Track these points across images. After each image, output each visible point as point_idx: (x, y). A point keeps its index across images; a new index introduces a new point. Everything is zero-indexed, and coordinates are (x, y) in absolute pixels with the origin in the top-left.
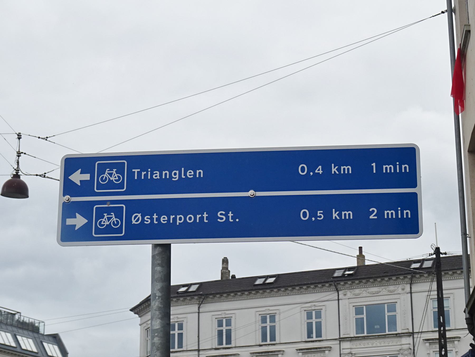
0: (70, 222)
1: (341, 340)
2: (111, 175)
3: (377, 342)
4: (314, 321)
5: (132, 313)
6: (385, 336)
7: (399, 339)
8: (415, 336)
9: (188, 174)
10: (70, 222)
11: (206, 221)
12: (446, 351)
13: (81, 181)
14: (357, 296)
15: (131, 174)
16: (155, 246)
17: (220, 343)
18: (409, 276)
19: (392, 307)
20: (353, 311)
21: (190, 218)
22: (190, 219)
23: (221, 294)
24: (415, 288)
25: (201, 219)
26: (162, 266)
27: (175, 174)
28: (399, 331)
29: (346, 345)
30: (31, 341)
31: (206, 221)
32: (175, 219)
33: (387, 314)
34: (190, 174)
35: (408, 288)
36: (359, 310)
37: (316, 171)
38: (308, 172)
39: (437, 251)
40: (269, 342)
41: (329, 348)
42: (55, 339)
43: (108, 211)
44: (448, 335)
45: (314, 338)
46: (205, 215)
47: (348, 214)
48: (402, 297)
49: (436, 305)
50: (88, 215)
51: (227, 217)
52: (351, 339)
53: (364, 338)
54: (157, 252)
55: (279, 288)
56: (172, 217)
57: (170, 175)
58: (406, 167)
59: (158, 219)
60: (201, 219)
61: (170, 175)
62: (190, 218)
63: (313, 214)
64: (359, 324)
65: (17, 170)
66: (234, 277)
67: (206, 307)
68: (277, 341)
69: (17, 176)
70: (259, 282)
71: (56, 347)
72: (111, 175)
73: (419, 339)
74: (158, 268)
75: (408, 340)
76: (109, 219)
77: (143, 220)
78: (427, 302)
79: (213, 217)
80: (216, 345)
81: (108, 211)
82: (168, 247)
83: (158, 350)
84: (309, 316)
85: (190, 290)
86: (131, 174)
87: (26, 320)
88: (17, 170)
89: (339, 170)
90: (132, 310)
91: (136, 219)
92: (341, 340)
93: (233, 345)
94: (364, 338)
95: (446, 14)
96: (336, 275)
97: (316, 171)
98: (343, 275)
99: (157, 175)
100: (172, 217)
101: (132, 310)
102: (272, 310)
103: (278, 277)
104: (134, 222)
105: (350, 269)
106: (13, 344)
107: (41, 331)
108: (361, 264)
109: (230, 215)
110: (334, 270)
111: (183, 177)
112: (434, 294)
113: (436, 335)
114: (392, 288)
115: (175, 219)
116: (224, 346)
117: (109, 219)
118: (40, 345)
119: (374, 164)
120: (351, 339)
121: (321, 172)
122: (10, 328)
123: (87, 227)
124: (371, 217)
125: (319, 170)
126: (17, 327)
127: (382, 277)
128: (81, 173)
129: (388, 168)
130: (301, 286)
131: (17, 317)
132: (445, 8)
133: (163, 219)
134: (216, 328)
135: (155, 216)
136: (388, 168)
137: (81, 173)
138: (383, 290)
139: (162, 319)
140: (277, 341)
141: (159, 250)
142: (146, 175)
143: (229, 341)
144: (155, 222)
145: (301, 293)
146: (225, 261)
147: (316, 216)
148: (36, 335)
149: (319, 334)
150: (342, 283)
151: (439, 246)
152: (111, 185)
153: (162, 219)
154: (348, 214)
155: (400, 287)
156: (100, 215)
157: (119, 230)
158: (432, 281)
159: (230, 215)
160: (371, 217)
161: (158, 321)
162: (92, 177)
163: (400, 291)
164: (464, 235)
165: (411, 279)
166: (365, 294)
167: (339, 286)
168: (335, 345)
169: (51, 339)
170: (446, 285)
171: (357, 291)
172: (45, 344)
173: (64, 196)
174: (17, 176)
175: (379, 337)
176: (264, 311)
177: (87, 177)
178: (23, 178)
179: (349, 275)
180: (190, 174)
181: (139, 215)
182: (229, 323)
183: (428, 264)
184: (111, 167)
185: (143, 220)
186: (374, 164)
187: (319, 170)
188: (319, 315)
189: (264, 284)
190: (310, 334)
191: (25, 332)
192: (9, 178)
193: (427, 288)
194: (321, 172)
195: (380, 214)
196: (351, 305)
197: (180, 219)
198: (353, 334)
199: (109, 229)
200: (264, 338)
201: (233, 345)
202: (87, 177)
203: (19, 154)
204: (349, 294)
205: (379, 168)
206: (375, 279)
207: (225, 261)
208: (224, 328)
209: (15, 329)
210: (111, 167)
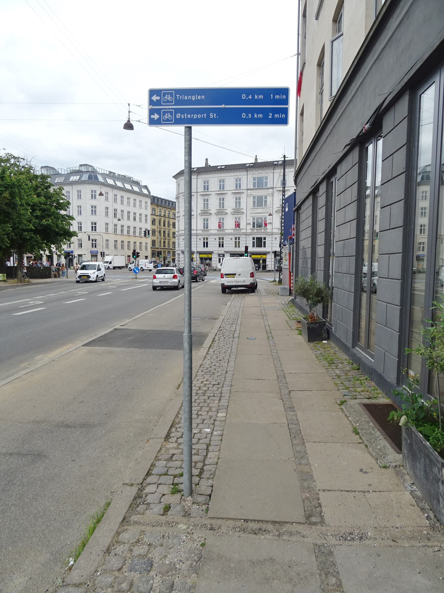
0: (152, 117)
1: (248, 190)
2: (168, 97)
3: (260, 191)
4: (238, 182)
5: (173, 178)
6: (263, 189)
7: (267, 190)
8: (274, 189)
9: (198, 97)
10: (152, 117)
11: (205, 117)
12: (285, 194)
13: (156, 100)
14: (254, 174)
15: (176, 97)
16: (186, 127)
17: (205, 190)
18: (273, 167)
19: (266, 178)
20: (252, 179)
21: (199, 116)
22: (199, 116)
23: (205, 172)
24: (275, 171)
25: (204, 116)
26: (189, 136)
27: (193, 97)
28: (268, 187)
29: (249, 191)
30: (137, 188)
31: (205, 117)
32: (193, 116)
33: (264, 181)
34: (199, 97)
35: (272, 171)
36: (254, 179)
37: (249, 98)
38: (246, 98)
39: (285, 157)
40: (222, 190)
41: (243, 193)
42: (146, 187)
43: (167, 112)
44: (286, 189)
45: (238, 189)
46: (205, 115)
47: (261, 116)
48: (270, 174)
49: (282, 177)
50: (159, 114)
51: (214, 116)
52: (251, 189)
53: (256, 189)
54: (186, 130)
55: (226, 170)
56: (192, 115)
57: (191, 97)
58: (284, 96)
59: (187, 116)
60: (204, 116)
61: (191, 97)
62: (199, 116)
63: (247, 115)
64: (254, 184)
65: (129, 119)
66: (210, 166)
67: (200, 177)
68: (225, 190)
69: (129, 121)
70: (219, 167)
71: (146, 190)
72: (168, 97)
73: (275, 190)
74: (187, 136)
75: (271, 190)
76: (168, 116)
77: (181, 116)
78: (279, 177)
79: (208, 116)
80: (203, 190)
81: (167, 112)
82: (190, 128)
83: (187, 168)
84: (237, 181)
85: (194, 170)
86: (176, 97)
87: (135, 180)
88: (129, 119)
89: (258, 97)
90: (173, 177)
91: (178, 116)
92: (248, 190)
93: (209, 191)
94: (256, 189)
95: (296, 56)
96: (247, 166)
97: (249, 98)
98: (250, 166)
99: (186, 98)
100: (192, 115)
101: (173, 177)
102: (223, 178)
103: (226, 166)
104: (177, 117)
105: (252, 163)
106: (131, 189)
107: (141, 184)
108: (256, 162)
109: (215, 115)
110: (246, 164)
111: (197, 99)
112: (282, 174)
113: (282, 189)
114: (267, 171)
115: (193, 116)
116: (206, 191)
117: (168, 116)
118: (140, 189)
119: (272, 95)
120: (251, 189)
121: (251, 98)
122: (129, 183)
123: (159, 119)
124: (269, 117)
125: (250, 97)
126: (132, 183)
127: (263, 167)
128: (156, 96)
129: (277, 97)
130: (234, 169)
131: (132, 179)
132: (296, 53)
133: (189, 116)
134: (203, 184)
135: (186, 115)
136: (277, 97)
137: (156, 96)
138: (264, 172)
139: (188, 156)
140: (225, 190)
141: (187, 129)
142: (182, 98)
143: (208, 189)
144: (186, 117)
145: (234, 172)
146: (207, 160)
147: (248, 116)
148: (139, 186)
149: (240, 187)
150: (249, 169)
151: (247, 245)
152: (168, 101)
153: (188, 116)
154: (261, 116)
155: (270, 171)
156: (164, 114)
157: (172, 121)
158: (281, 169)
159: (215, 115)
160: (269, 117)
161: (187, 157)
162: (161, 98)
163: (269, 172)
164: (296, 148)
165: (274, 168)
166: (257, 173)
167: (248, 170)
168: (245, 191)
169: (144, 187)
170: (286, 170)
171: (254, 172)
172: (142, 189)
173: (150, 105)
174: (129, 121)
175: (261, 189)
176: (220, 178)
177: (158, 98)
178: (131, 122)
179: (252, 166)
180: (199, 97)
181: (179, 114)
182: (208, 183)
183: (280, 162)
184: (168, 94)
185: (181, 116)
186: (272, 95)
187: (250, 97)
188: (240, 180)
189: (221, 168)
190: (236, 187)
191: (135, 185)
192: (126, 122)
193: (279, 172)
194: (251, 98)
195: (273, 116)
196: (252, 177)
197: (195, 116)
198: (252, 188)
199: (167, 120)
200: (220, 188)
201: (209, 191)
202: (158, 98)
203: (129, 112)
204: (251, 173)
205: (274, 97)
206: (261, 167)
207: (207, 160)
208: (206, 184)
209: (131, 183)
210: (168, 94)
